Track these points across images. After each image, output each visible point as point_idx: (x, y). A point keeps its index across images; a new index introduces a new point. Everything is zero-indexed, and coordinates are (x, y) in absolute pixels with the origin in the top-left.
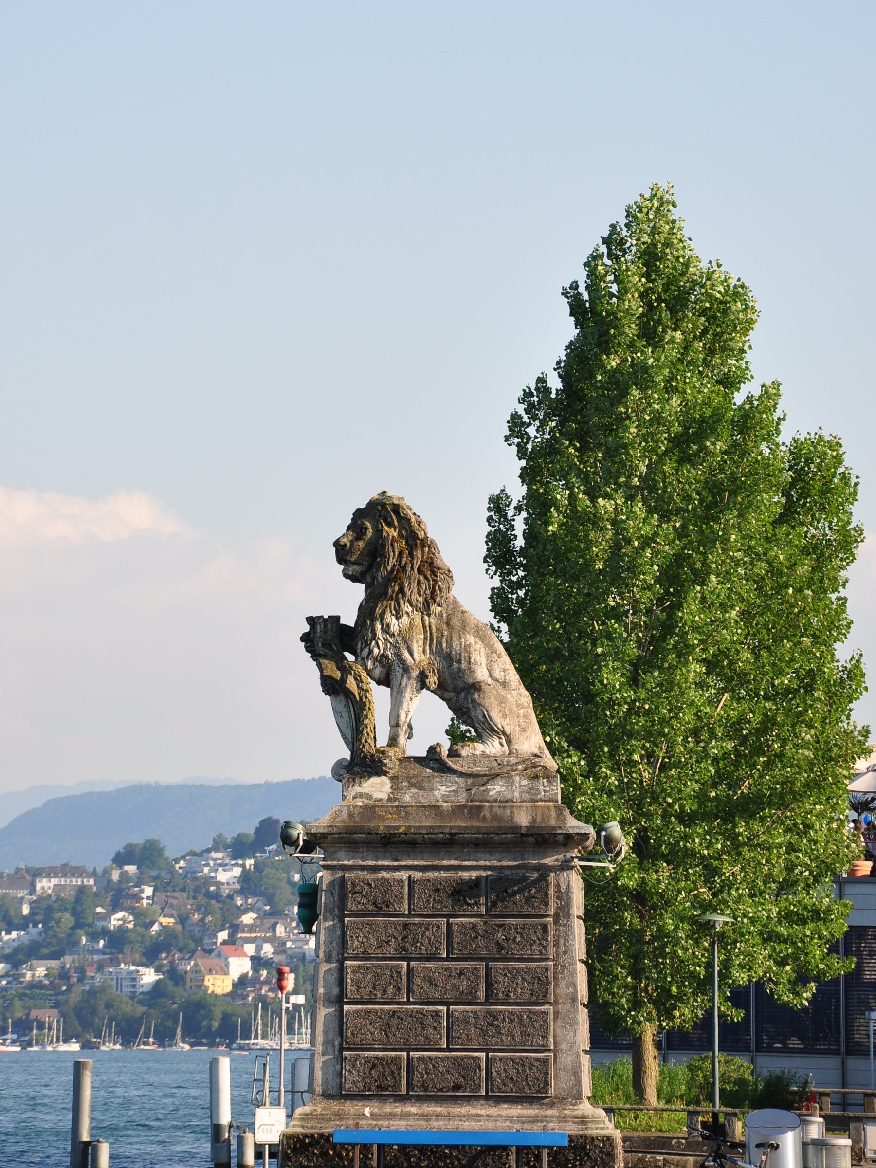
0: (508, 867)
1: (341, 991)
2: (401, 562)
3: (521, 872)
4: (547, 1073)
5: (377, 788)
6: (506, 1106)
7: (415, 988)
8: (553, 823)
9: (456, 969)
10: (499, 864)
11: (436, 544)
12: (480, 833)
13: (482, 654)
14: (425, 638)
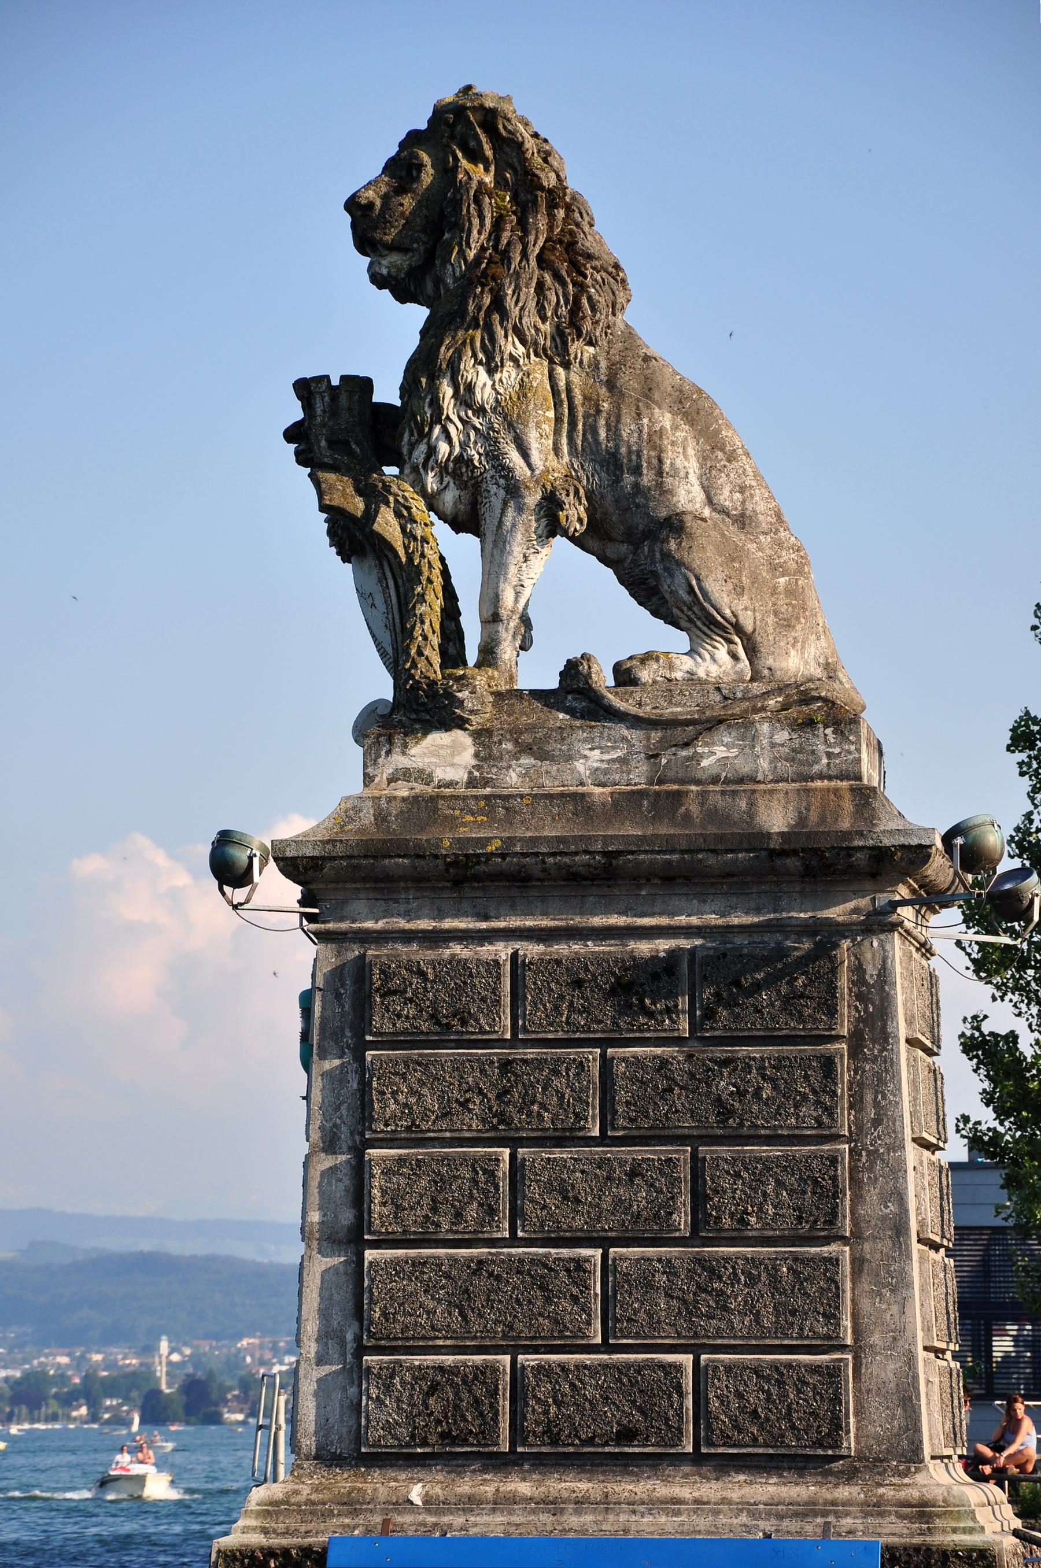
0: (743, 929)
1: (359, 1218)
2: (497, 240)
3: (771, 940)
4: (837, 1400)
5: (444, 757)
6: (742, 1477)
7: (528, 1206)
8: (845, 824)
9: (622, 1163)
10: (721, 922)
11: (584, 203)
12: (672, 851)
13: (691, 451)
14: (558, 420)
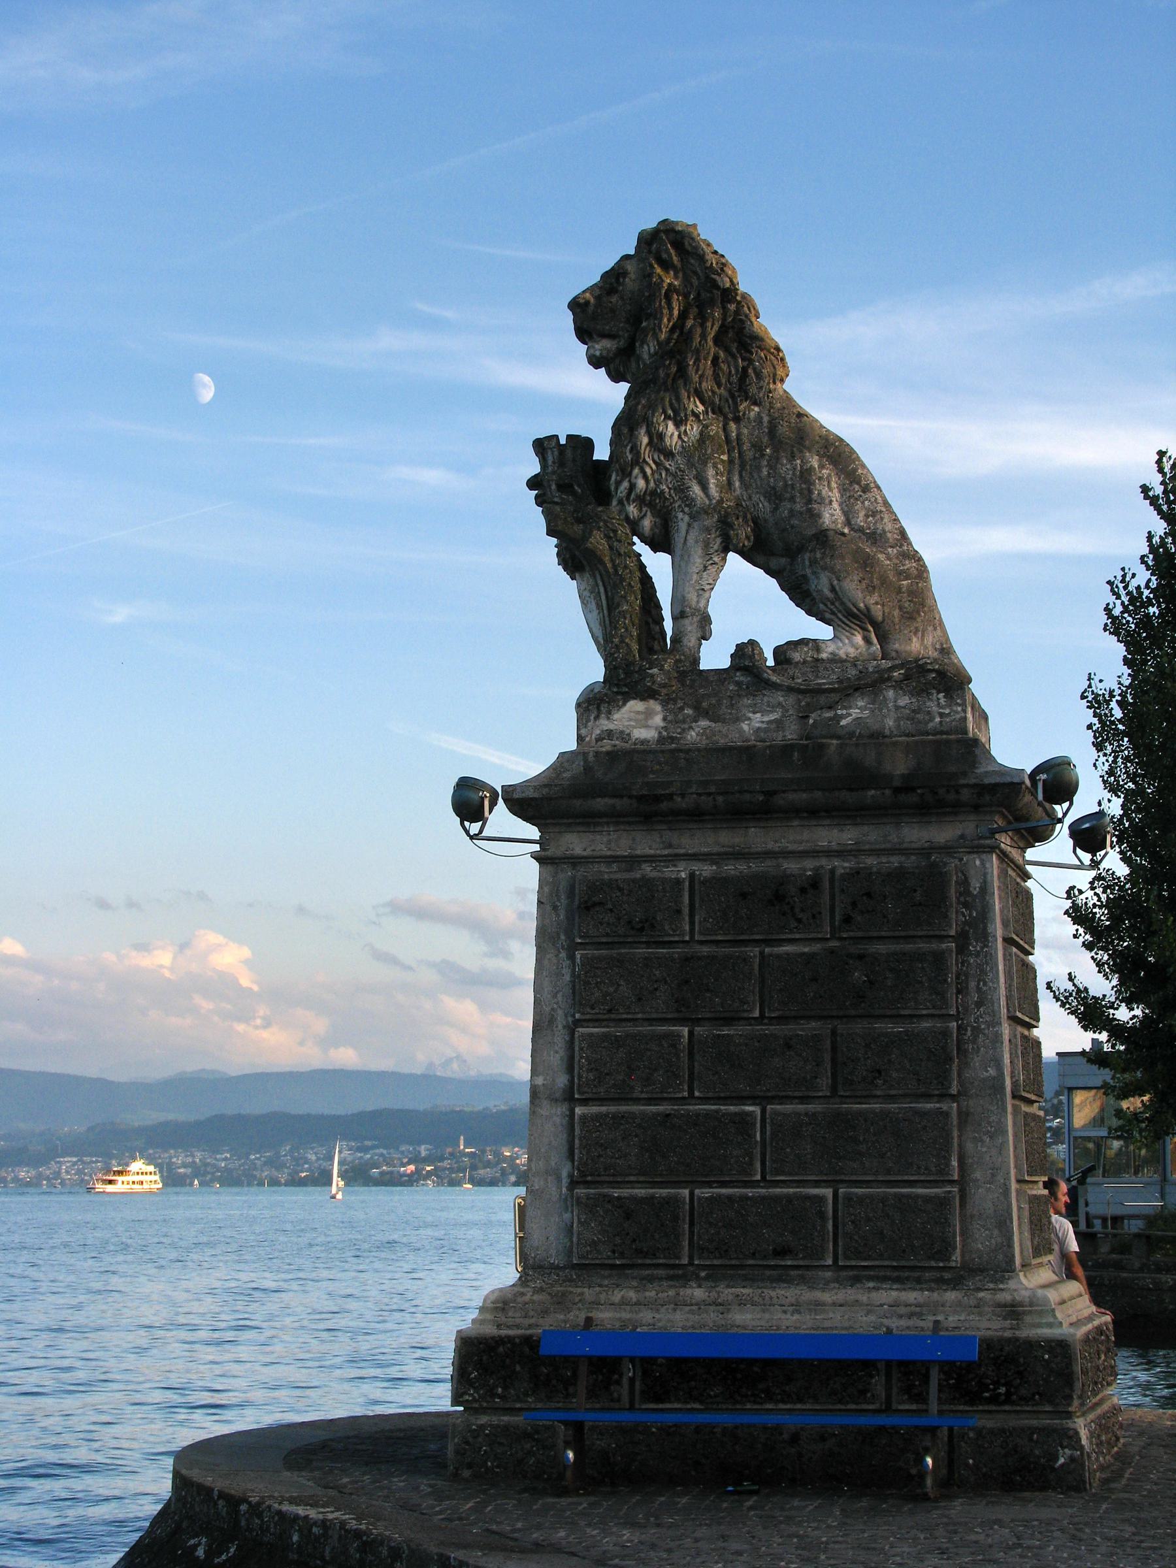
13: (834, 485)
